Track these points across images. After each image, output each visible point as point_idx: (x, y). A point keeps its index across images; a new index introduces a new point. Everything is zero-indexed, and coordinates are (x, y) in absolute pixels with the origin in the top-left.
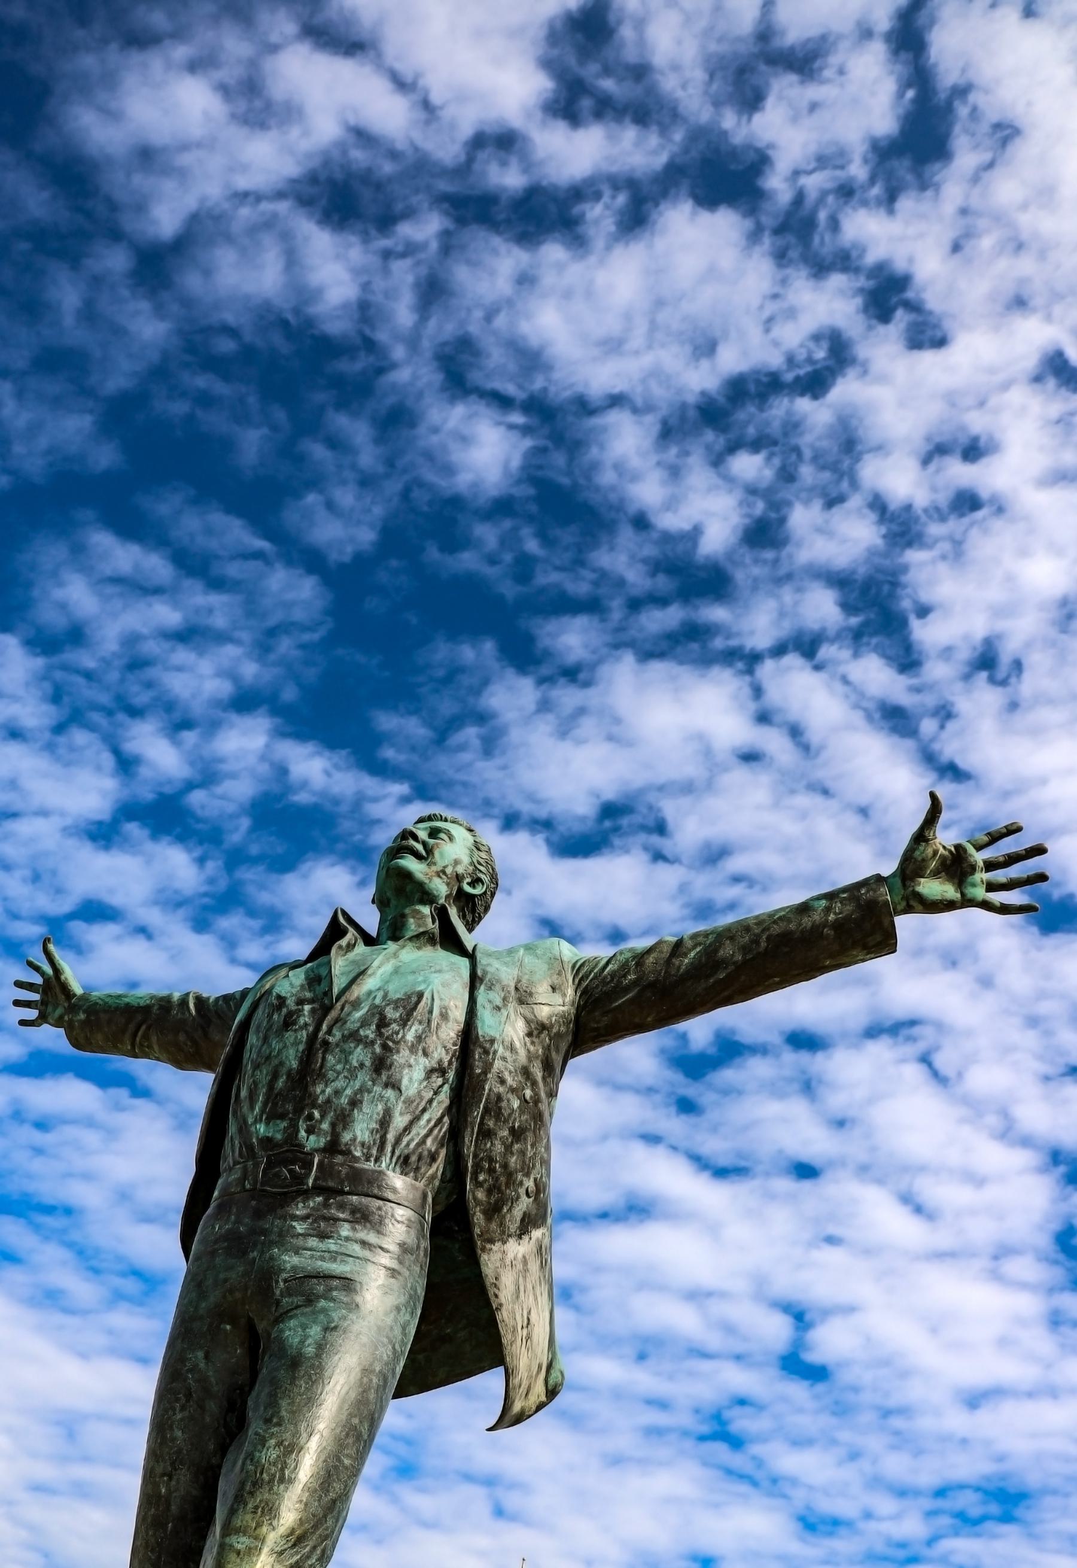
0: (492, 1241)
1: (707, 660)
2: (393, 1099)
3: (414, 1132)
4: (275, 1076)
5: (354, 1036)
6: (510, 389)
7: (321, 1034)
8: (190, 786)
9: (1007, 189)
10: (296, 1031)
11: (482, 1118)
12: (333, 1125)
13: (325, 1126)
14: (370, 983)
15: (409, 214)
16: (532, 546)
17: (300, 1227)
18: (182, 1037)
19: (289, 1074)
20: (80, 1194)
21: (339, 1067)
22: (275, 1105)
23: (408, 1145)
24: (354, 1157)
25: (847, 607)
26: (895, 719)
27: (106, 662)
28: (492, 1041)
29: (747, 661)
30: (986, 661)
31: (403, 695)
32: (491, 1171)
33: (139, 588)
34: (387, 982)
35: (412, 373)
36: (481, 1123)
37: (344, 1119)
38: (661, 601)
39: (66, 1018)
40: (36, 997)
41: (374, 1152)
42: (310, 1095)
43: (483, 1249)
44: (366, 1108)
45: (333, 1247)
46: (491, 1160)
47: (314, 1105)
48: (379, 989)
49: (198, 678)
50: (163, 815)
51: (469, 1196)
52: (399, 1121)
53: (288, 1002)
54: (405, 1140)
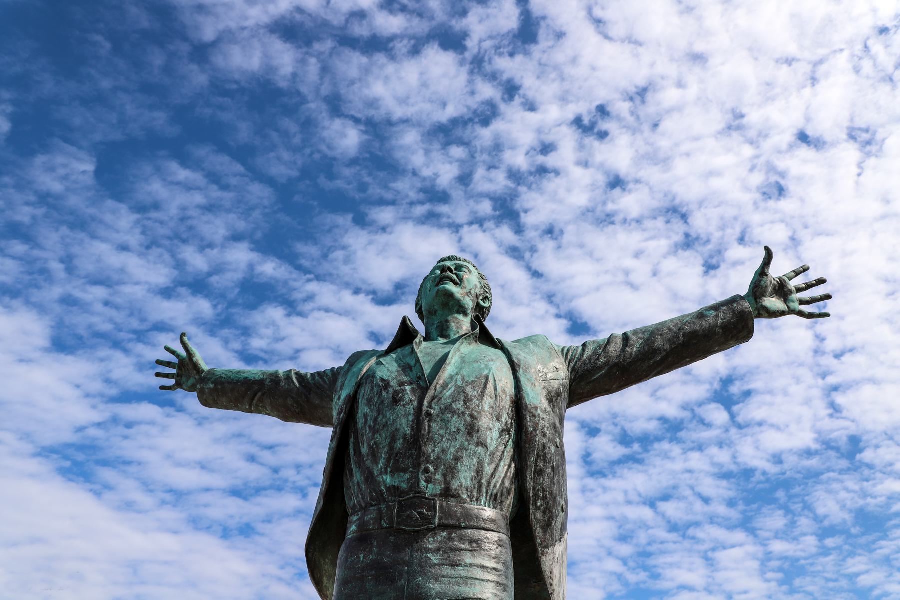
0: (547, 547)
1: (440, 227)
2: (483, 453)
3: (497, 476)
4: (394, 439)
5: (448, 409)
6: (359, 116)
7: (424, 409)
8: (210, 274)
9: (560, 56)
10: (404, 405)
11: (536, 462)
12: (445, 476)
13: (439, 477)
14: (449, 370)
15: (319, 39)
16: (367, 179)
17: (435, 559)
18: (290, 402)
19: (405, 438)
21: (442, 432)
22: (397, 461)
23: (495, 486)
24: (462, 499)
25: (495, 209)
26: (514, 253)
27: (172, 219)
28: (536, 408)
29: (456, 228)
30: (550, 231)
31: (308, 237)
32: (545, 498)
33: (188, 188)
34: (461, 369)
35: (314, 106)
36: (536, 466)
37: (451, 471)
38: (422, 203)
39: (199, 387)
40: (174, 371)
41: (475, 494)
42: (424, 454)
43: (543, 554)
44: (466, 462)
45: (463, 574)
46: (544, 491)
47: (428, 462)
48: (457, 374)
49: (216, 228)
51: (532, 517)
52: (488, 470)
53: (392, 384)
54: (494, 482)
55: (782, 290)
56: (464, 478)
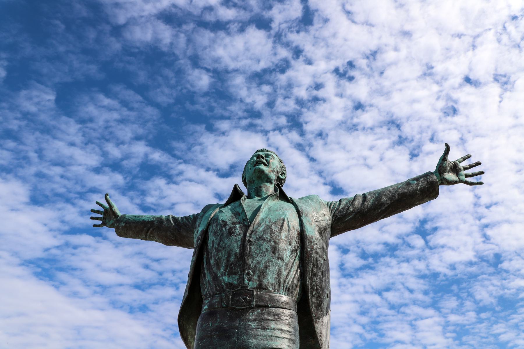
0: (319, 318)
1: (256, 132)
2: (281, 264)
3: (289, 277)
4: (229, 255)
5: (261, 238)
6: (209, 67)
7: (247, 238)
8: (122, 160)
9: (326, 33)
10: (235, 236)
11: (312, 269)
12: (259, 277)
13: (255, 277)
14: (261, 215)
15: (186, 23)
16: (214, 104)
17: (253, 325)
19: (236, 255)
20: (85, 265)
21: (257, 251)
22: (231, 268)
23: (288, 283)
24: (269, 290)
25: (288, 122)
26: (300, 147)
27: (100, 127)
28: (312, 237)
29: (265, 133)
30: (320, 135)
31: (180, 138)
32: (317, 290)
33: (110, 109)
34: (268, 215)
35: (183, 62)
36: (312, 271)
37: (263, 274)
38: (246, 118)
41: (277, 287)
42: (247, 264)
43: (316, 322)
44: (271, 269)
45: (270, 334)
46: (317, 285)
47: (249, 269)
48: (266, 218)
49: (126, 133)
50: (116, 166)
51: (310, 301)
52: (284, 273)
53: (228, 223)
54: (287, 280)
55: (455, 169)
56: (270, 278)
